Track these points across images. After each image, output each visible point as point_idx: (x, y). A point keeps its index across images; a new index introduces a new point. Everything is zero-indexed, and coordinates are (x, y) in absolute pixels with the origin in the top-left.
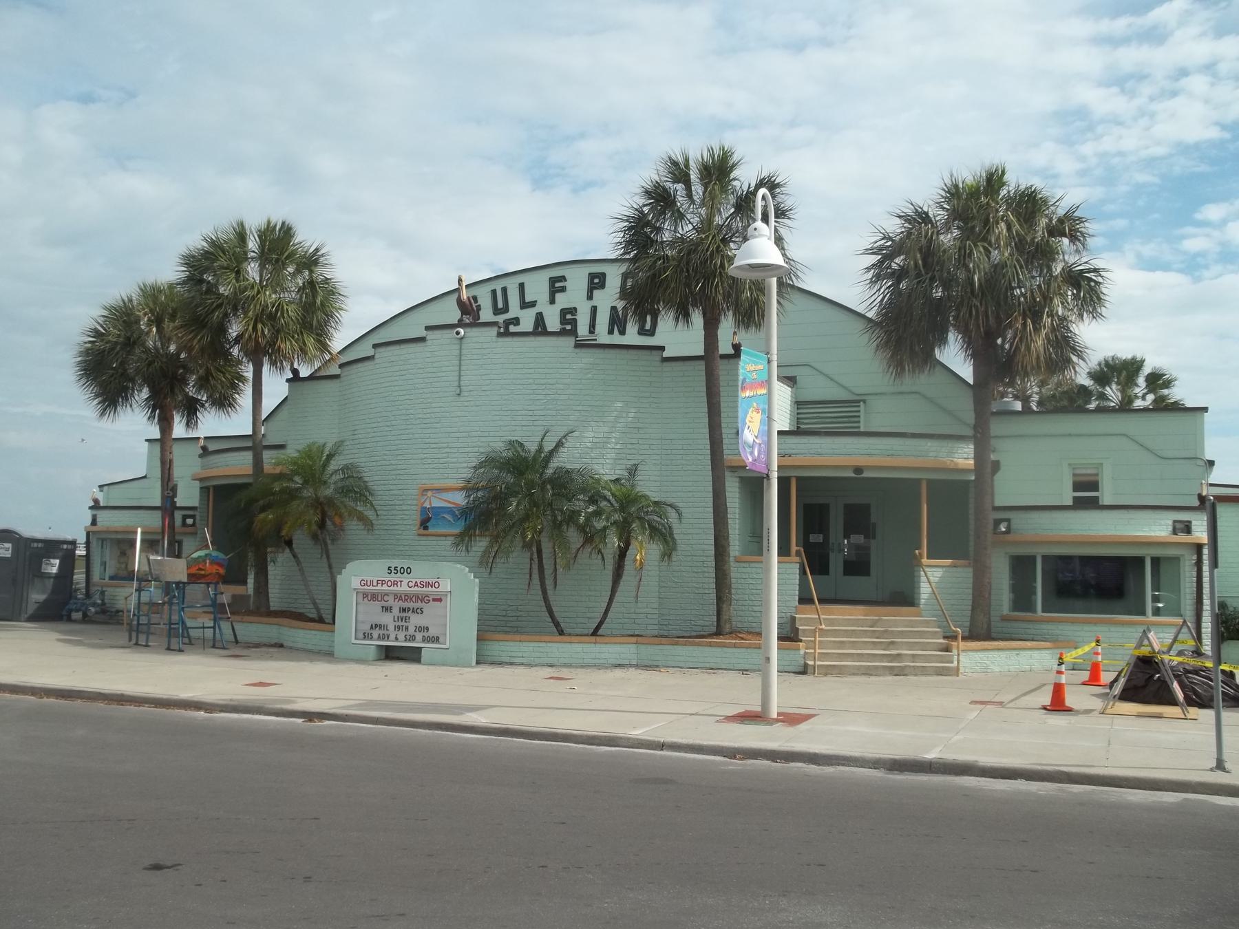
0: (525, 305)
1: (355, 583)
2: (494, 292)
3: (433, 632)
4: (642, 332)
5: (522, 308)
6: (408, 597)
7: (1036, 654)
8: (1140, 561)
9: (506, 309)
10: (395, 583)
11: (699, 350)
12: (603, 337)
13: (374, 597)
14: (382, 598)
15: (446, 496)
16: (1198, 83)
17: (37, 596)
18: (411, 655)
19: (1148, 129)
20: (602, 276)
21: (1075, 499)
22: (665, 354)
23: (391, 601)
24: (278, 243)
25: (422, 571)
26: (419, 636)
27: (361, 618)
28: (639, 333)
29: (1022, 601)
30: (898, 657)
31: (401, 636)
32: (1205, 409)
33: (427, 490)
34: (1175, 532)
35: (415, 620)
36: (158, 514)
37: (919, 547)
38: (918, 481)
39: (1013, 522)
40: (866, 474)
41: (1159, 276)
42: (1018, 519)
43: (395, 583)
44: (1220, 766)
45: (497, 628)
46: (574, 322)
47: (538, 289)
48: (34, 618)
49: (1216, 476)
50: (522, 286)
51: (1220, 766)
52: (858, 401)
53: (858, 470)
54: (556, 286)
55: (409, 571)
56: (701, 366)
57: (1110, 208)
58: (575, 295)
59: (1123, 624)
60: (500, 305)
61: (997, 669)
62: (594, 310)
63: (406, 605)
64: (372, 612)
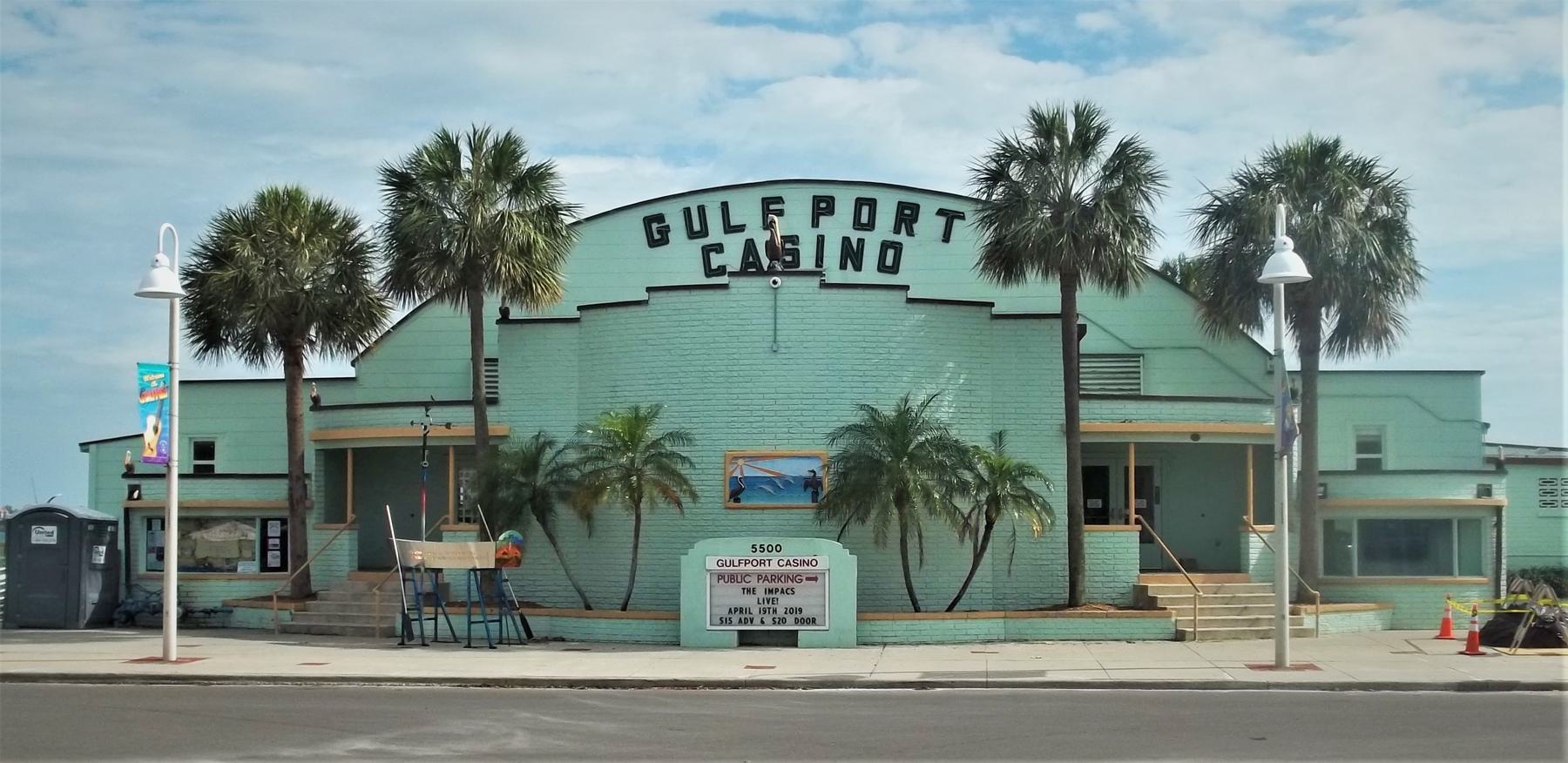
0: (729, 228)
1: (711, 564)
2: (687, 211)
3: (806, 614)
4: (882, 268)
5: (726, 232)
6: (776, 577)
7: (1364, 615)
8: (1447, 523)
9: (704, 232)
10: (761, 562)
12: (834, 273)
13: (732, 578)
14: (743, 579)
15: (760, 464)
17: (92, 594)
18: (789, 640)
20: (830, 201)
21: (196, 467)
22: (995, 310)
23: (753, 583)
25: (795, 548)
26: (790, 618)
27: (715, 601)
28: (879, 270)
30: (1256, 621)
32: (1482, 373)
33: (736, 458)
34: (1479, 496)
35: (784, 602)
37: (1246, 513)
39: (1330, 487)
40: (1202, 440)
42: (1332, 482)
43: (761, 562)
46: (795, 253)
47: (747, 210)
48: (88, 626)
49: (1489, 437)
50: (725, 206)
52: (1138, 356)
53: (1195, 436)
54: (771, 207)
55: (778, 548)
56: (1058, 324)
59: (1436, 584)
60: (697, 227)
61: (1334, 630)
62: (821, 240)
63: (773, 585)
64: (733, 596)
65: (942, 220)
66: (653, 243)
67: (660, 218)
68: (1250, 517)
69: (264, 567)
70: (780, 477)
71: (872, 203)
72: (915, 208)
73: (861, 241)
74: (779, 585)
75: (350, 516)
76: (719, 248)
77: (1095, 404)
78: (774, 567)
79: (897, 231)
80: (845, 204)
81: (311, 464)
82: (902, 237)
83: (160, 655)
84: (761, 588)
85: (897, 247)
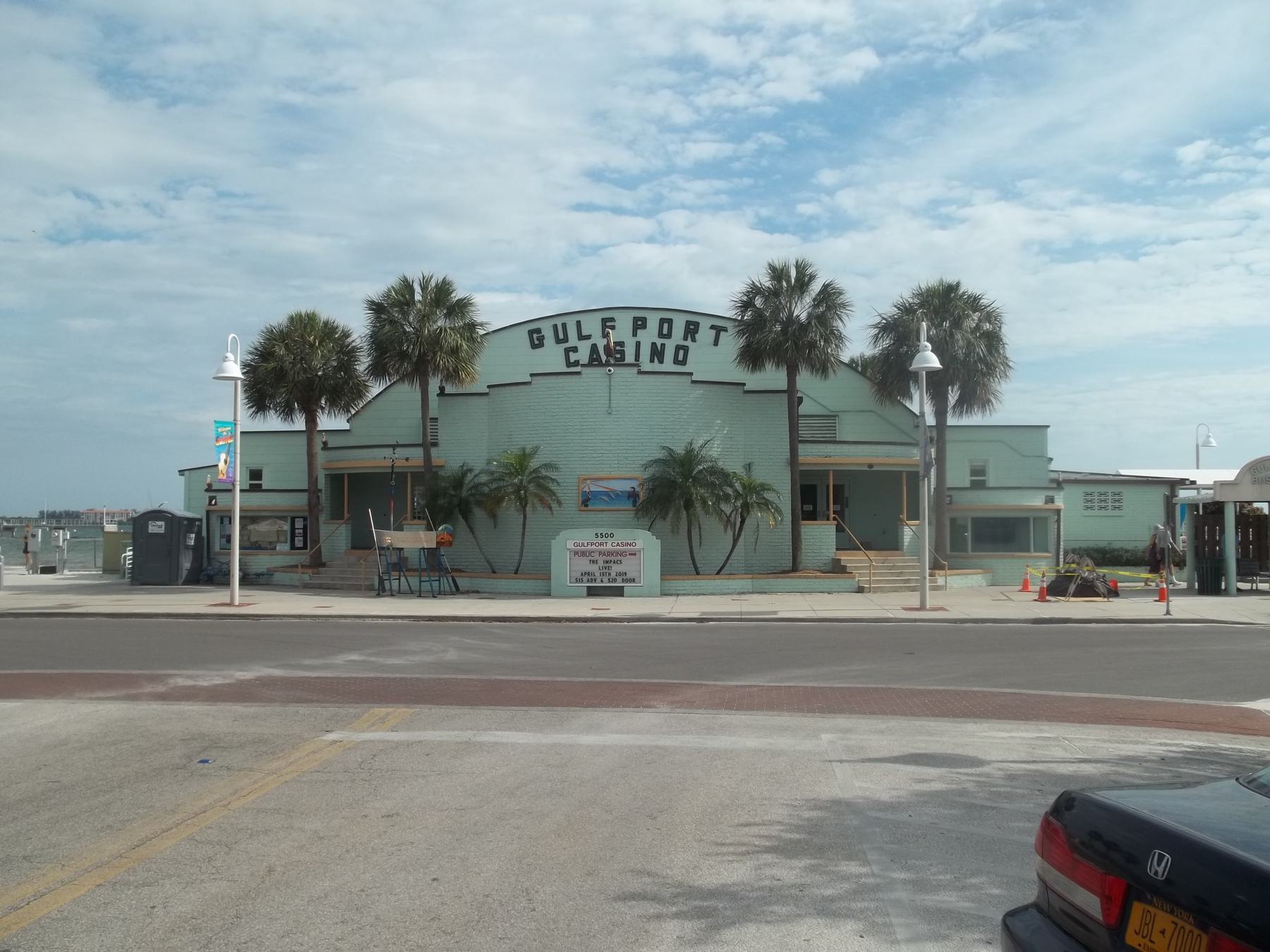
0: (582, 337)
1: (570, 545)
2: (555, 326)
3: (628, 576)
6: (610, 553)
9: (566, 340)
10: (601, 544)
11: (785, 387)
12: (646, 365)
13: (583, 554)
15: (601, 483)
16: (808, 44)
19: (758, 86)
20: (644, 320)
21: (972, 481)
23: (596, 557)
24: (441, 295)
26: (619, 579)
29: (958, 545)
30: (908, 581)
31: (605, 579)
35: (616, 568)
36: (305, 495)
38: (901, 472)
41: (777, 238)
43: (601, 544)
44: (1168, 613)
45: (669, 570)
46: (622, 353)
47: (592, 326)
48: (187, 582)
49: (1053, 466)
50: (579, 323)
51: (1168, 613)
53: (870, 466)
55: (612, 535)
57: (737, 166)
58: (623, 332)
59: (1020, 557)
60: (561, 336)
62: (638, 344)
63: (609, 558)
64: (584, 565)
65: (713, 332)
66: (534, 346)
67: (538, 331)
68: (904, 516)
69: (293, 547)
70: (613, 491)
71: (670, 321)
72: (697, 325)
73: (663, 345)
74: (613, 558)
75: (346, 515)
76: (575, 349)
77: (809, 447)
78: (609, 547)
79: (685, 339)
80: (653, 324)
81: (322, 483)
82: (688, 343)
83: (228, 601)
84: (601, 560)
85: (686, 349)
